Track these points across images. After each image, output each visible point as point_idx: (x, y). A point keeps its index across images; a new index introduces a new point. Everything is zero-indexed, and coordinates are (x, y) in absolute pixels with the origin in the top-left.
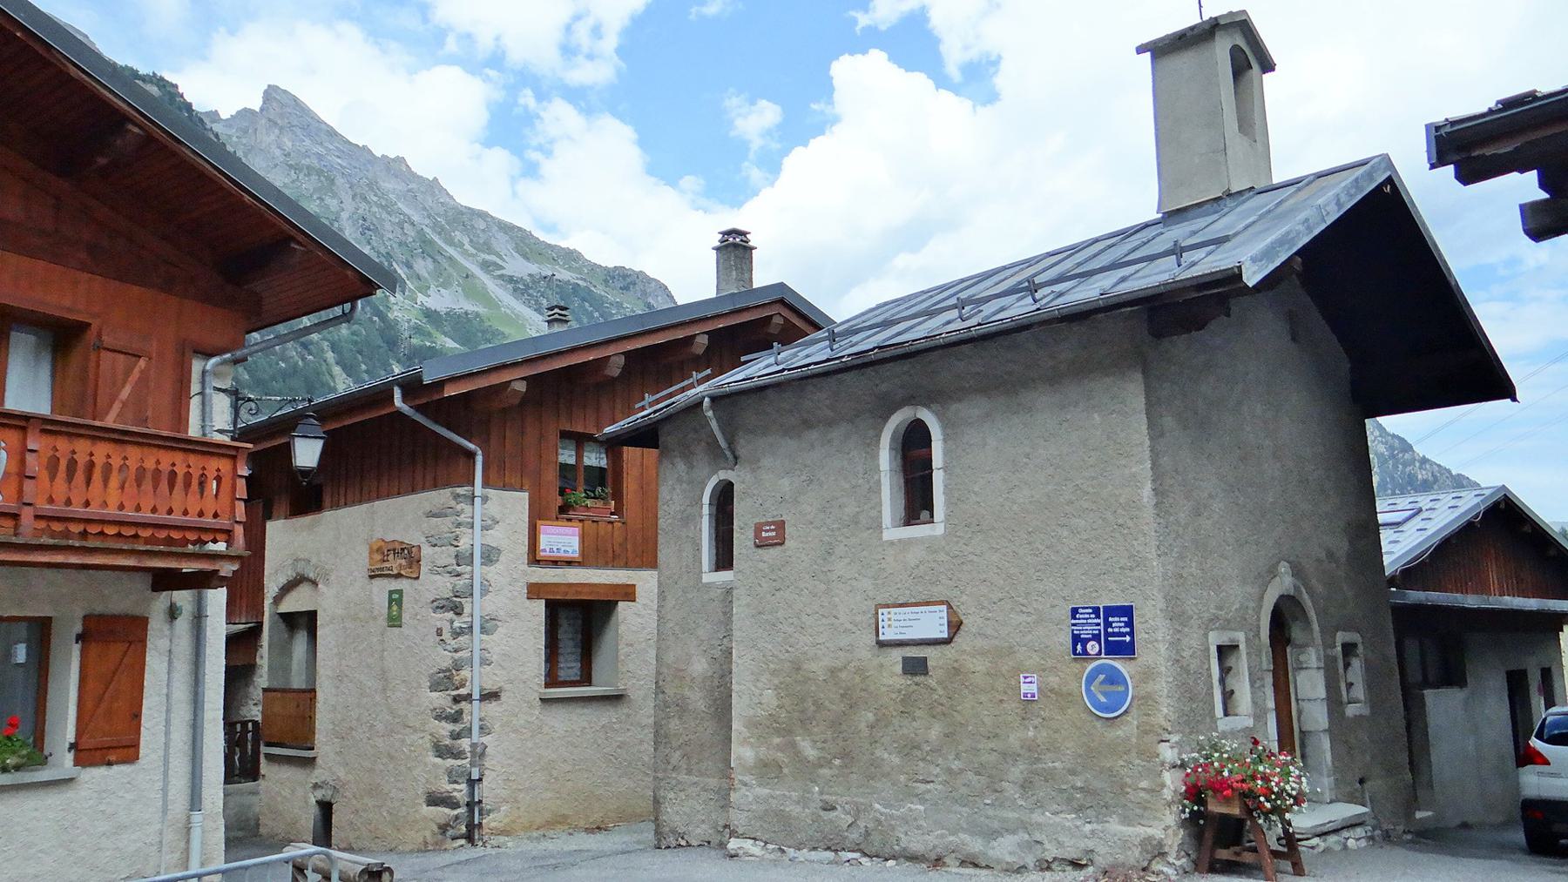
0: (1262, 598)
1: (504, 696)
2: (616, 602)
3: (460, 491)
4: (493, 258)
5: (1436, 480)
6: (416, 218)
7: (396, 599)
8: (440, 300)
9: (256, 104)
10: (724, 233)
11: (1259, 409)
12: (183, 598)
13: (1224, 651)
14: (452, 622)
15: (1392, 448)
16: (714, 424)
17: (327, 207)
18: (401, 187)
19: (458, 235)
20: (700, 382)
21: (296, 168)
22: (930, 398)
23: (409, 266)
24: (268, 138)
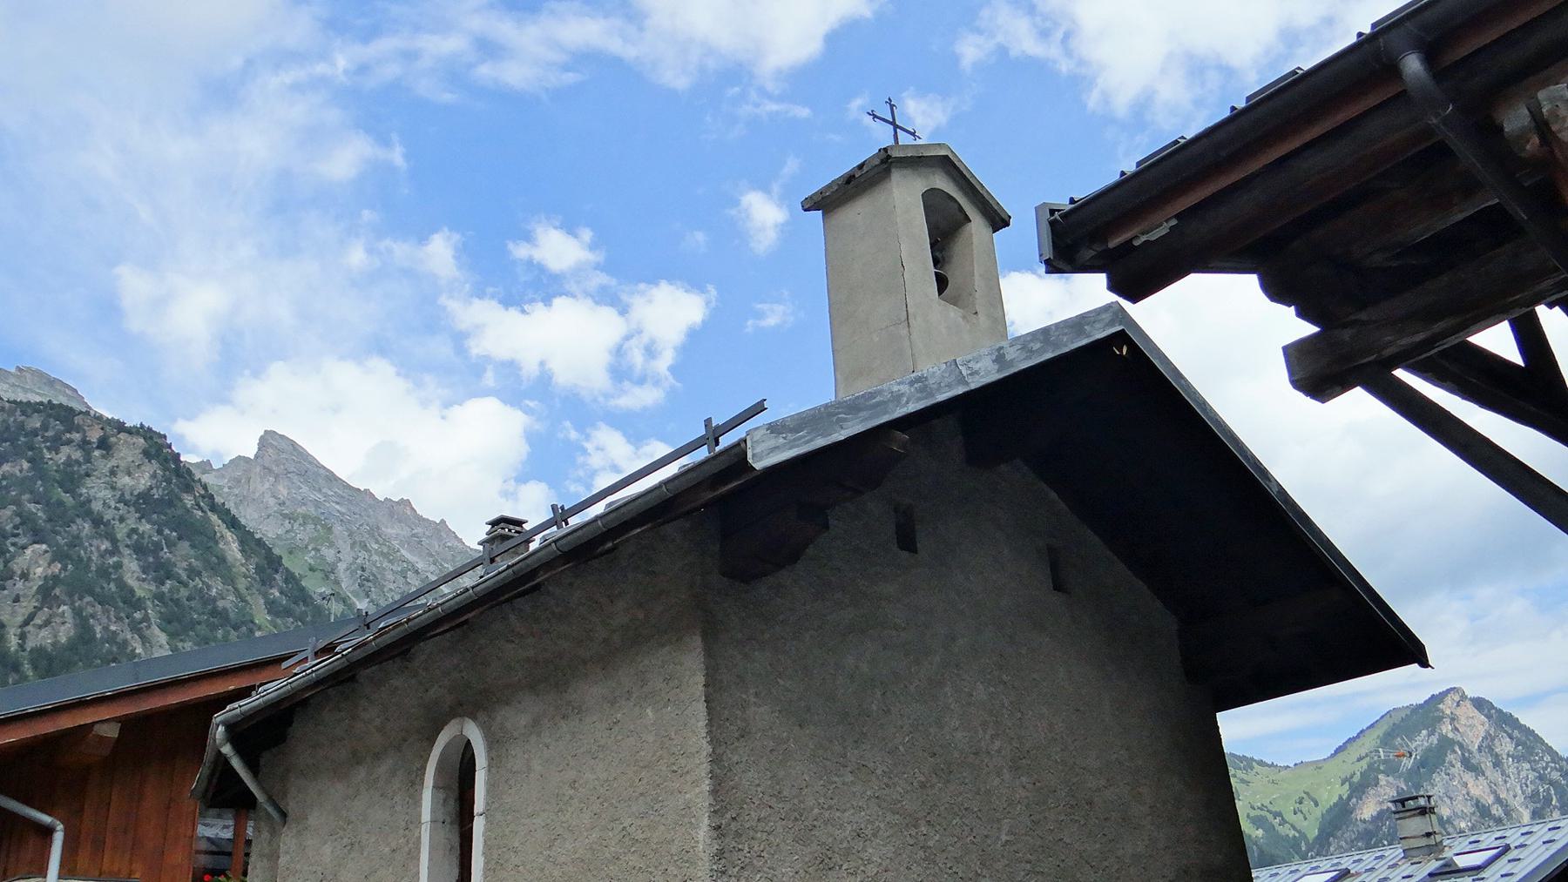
6: (420, 565)
9: (251, 451)
10: (494, 523)
11: (981, 692)
17: (323, 558)
18: (406, 532)
21: (291, 518)
22: (475, 703)
24: (261, 486)
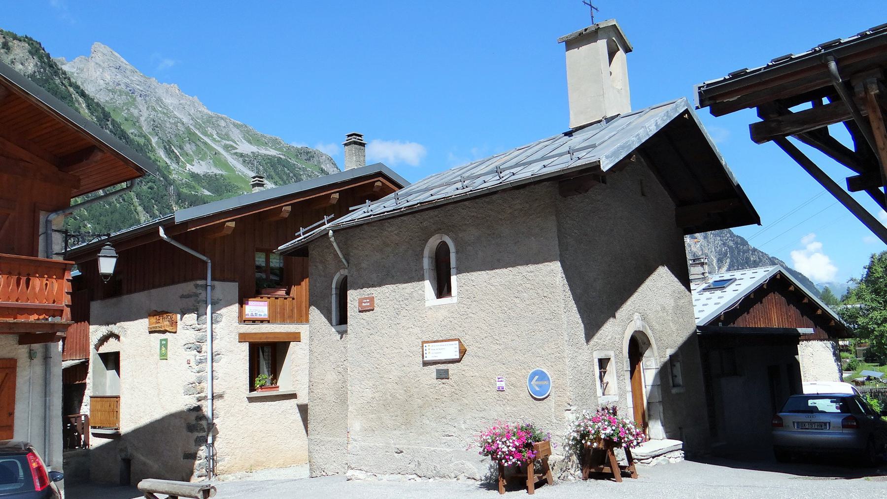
0: (624, 333)
1: (226, 397)
2: (289, 342)
3: (200, 282)
4: (231, 143)
5: (761, 260)
6: (185, 120)
7: (164, 344)
8: (200, 168)
10: (349, 136)
12: (37, 347)
13: (603, 363)
14: (196, 356)
15: (736, 243)
16: (335, 244)
17: (132, 114)
19: (210, 130)
20: (329, 222)
21: (113, 91)
23: (181, 148)
